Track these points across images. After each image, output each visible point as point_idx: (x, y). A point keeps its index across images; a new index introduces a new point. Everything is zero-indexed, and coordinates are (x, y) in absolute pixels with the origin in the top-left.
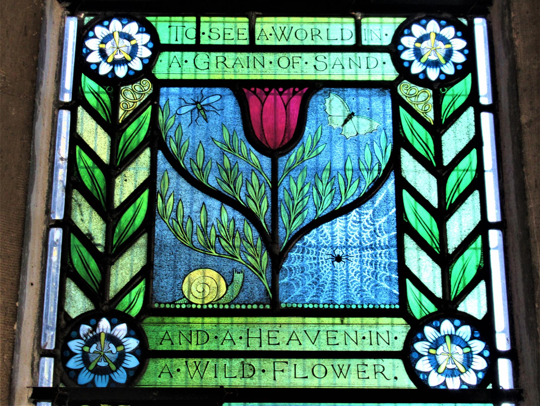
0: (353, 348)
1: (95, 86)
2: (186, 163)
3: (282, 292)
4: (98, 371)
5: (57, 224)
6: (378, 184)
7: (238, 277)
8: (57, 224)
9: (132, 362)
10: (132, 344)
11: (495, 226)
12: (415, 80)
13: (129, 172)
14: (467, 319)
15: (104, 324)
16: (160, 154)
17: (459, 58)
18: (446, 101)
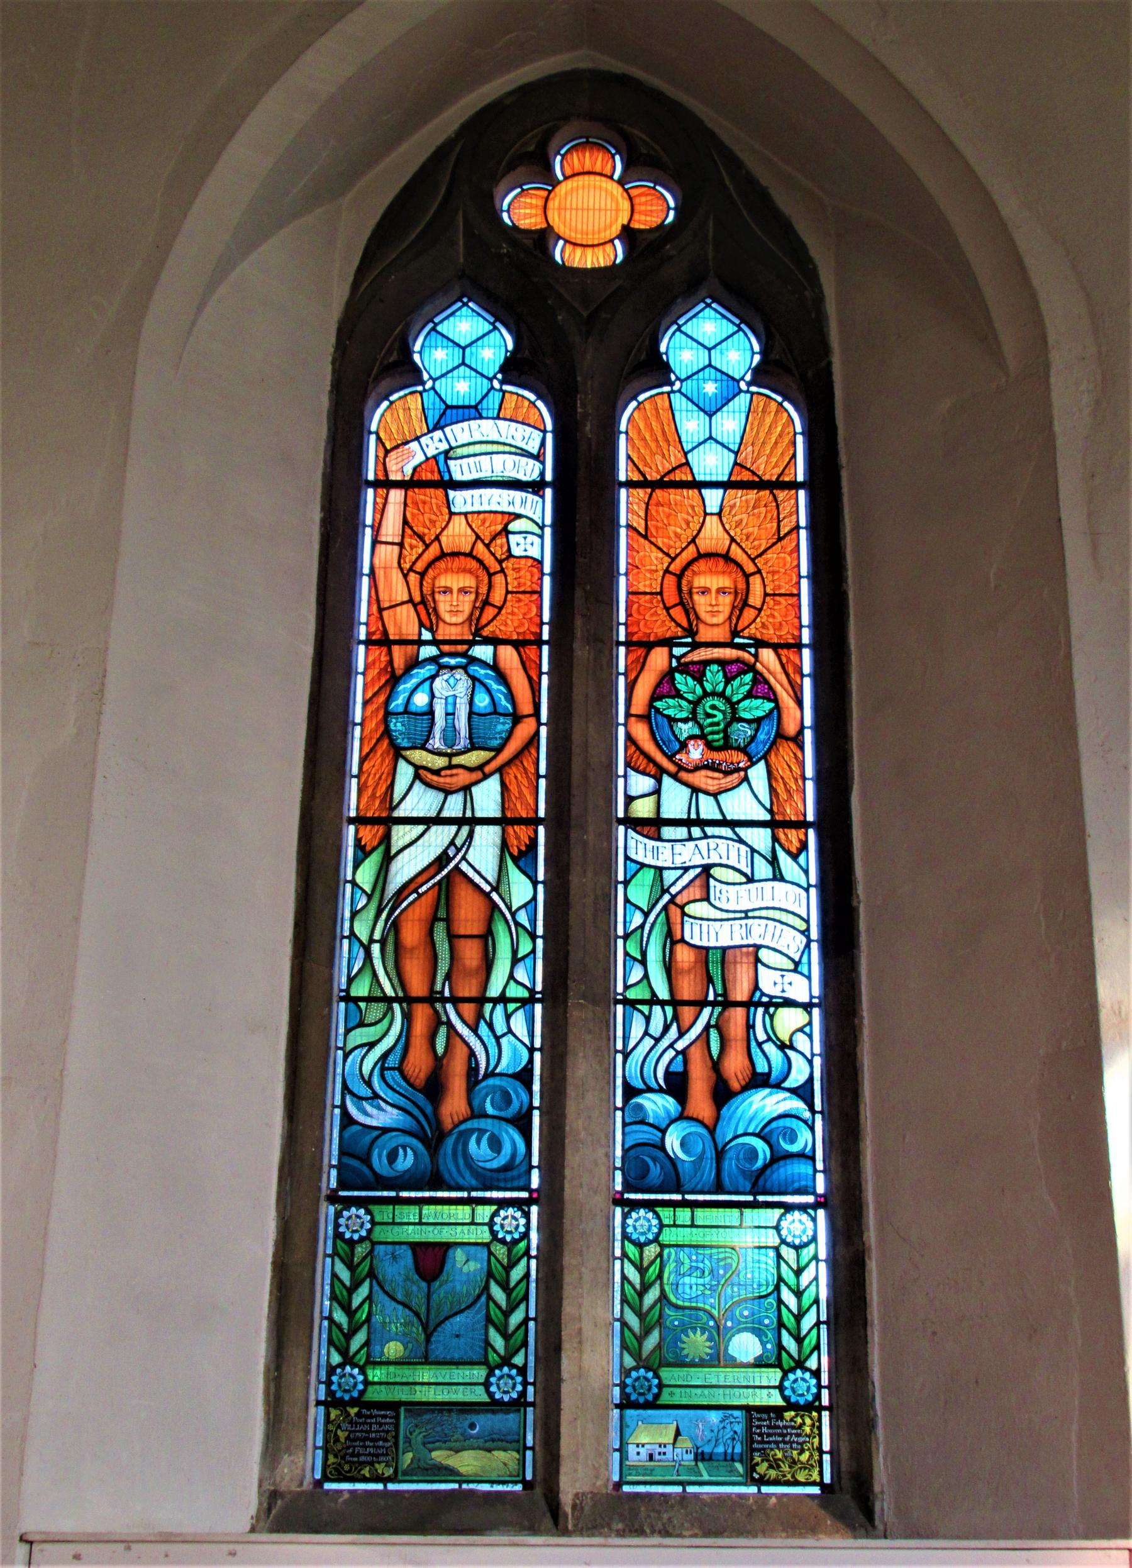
0: (461, 1381)
1: (343, 1245)
2: (387, 1288)
3: (430, 1353)
4: (345, 1391)
5: (326, 1318)
6: (479, 1297)
7: (410, 1345)
8: (326, 1318)
9: (361, 1387)
10: (361, 1378)
11: (824, 1323)
12: (788, 1245)
13: (360, 1290)
14: (515, 1366)
15: (348, 1368)
16: (374, 1282)
17: (522, 1229)
18: (515, 1251)
